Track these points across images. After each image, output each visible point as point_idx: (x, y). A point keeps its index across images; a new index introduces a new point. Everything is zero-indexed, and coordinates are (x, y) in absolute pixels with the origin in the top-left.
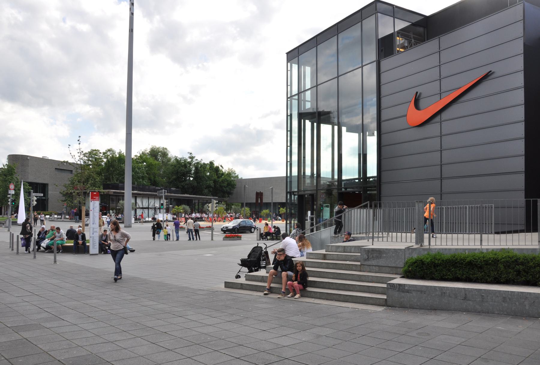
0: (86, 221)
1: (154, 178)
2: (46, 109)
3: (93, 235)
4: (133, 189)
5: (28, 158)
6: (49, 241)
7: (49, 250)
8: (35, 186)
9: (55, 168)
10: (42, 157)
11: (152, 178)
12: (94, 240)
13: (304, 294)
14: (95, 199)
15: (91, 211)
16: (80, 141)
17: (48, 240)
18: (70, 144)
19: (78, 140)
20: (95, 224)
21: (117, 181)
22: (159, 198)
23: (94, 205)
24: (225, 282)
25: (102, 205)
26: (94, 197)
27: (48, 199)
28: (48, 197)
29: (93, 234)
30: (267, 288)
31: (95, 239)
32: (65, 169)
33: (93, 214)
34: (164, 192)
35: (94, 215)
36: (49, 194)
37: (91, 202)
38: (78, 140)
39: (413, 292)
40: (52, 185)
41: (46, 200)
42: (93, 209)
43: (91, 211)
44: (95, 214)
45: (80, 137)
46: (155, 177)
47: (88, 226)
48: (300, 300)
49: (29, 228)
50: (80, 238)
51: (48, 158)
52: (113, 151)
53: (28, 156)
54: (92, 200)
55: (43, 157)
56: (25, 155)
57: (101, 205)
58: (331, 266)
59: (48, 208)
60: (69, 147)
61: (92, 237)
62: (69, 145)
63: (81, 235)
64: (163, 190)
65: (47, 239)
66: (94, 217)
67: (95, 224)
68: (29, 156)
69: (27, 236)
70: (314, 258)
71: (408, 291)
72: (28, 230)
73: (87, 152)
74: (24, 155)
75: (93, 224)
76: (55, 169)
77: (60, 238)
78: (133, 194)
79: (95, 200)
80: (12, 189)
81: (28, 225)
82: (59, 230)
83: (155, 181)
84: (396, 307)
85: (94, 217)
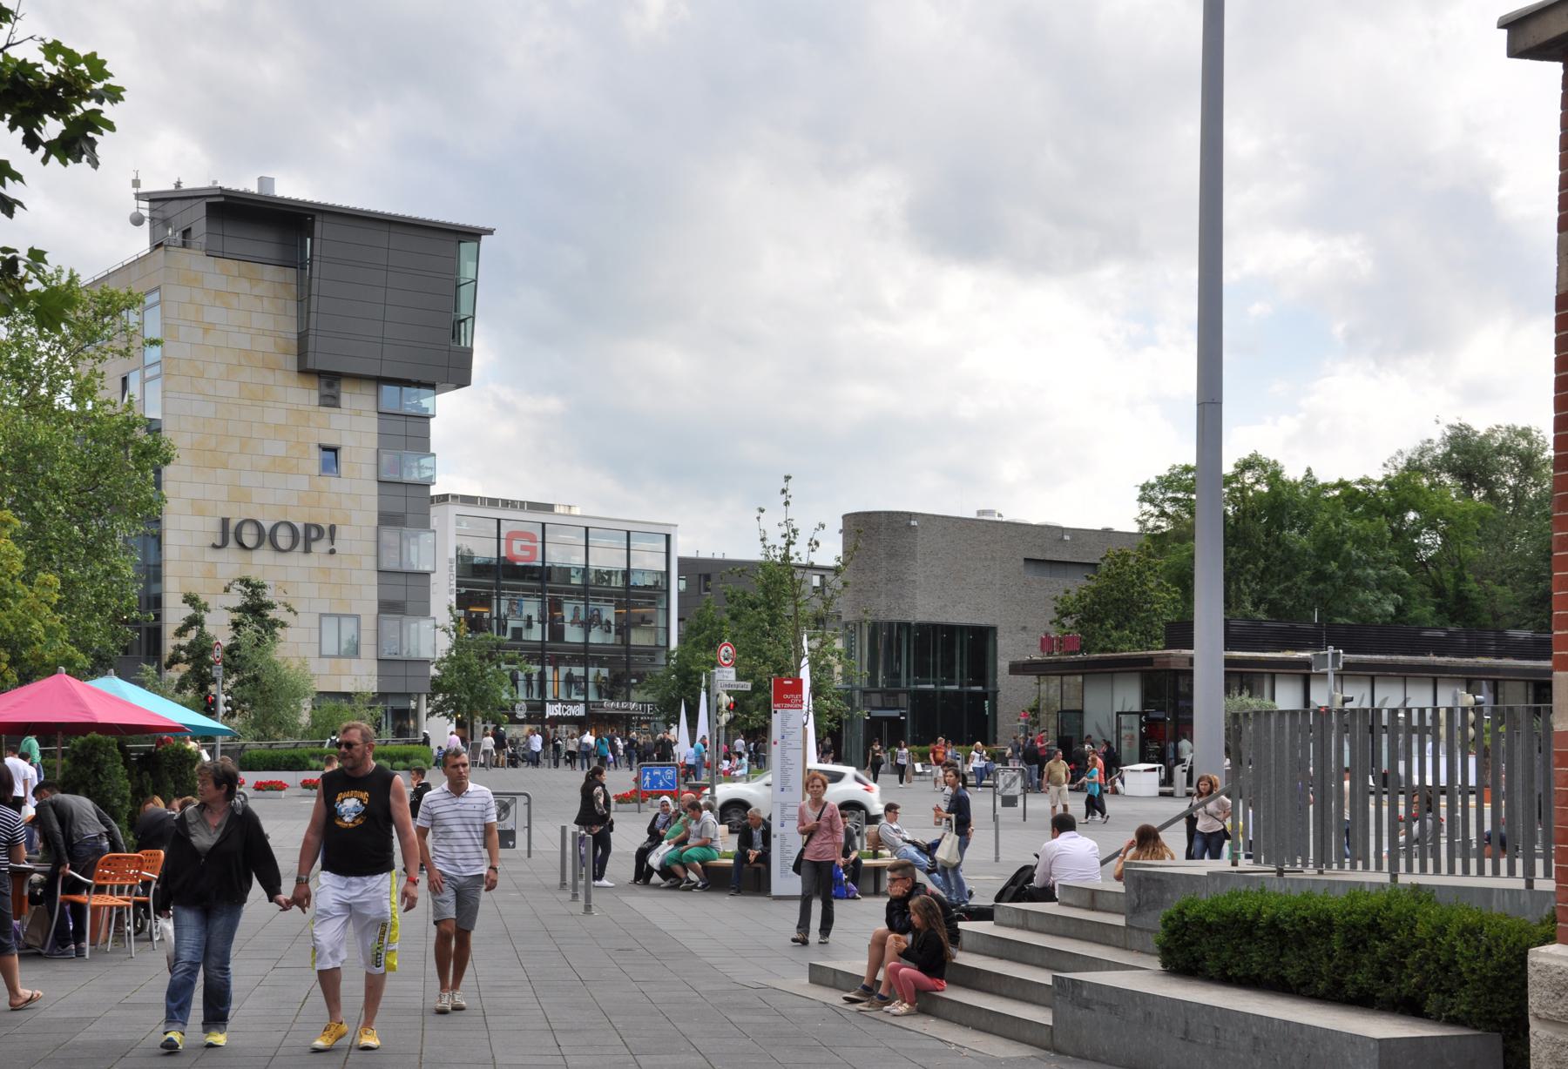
0: (1007, 786)
1: (1457, 585)
2: (1110, 273)
3: (783, 830)
4: (1231, 641)
5: (914, 523)
6: (672, 846)
7: (672, 880)
8: (969, 639)
9: (1025, 559)
10: (973, 516)
11: (1446, 585)
12: (788, 848)
13: (925, 1004)
14: (788, 701)
15: (775, 743)
16: (789, 493)
17: (669, 844)
18: (763, 507)
19: (784, 491)
20: (791, 790)
21: (1256, 605)
22: (1369, 678)
23: (784, 724)
24: (811, 964)
25: (1151, 716)
26: (786, 696)
27: (995, 693)
28: (995, 684)
29: (782, 825)
30: (864, 983)
31: (787, 843)
32: (1067, 558)
33: (783, 754)
34: (1333, 654)
35: (784, 759)
36: (999, 673)
37: (775, 712)
38: (784, 491)
39: (1096, 1007)
40: (1010, 632)
41: (990, 695)
42: (783, 737)
43: (775, 743)
44: (789, 754)
45: (788, 478)
46: (1461, 578)
47: (1013, 806)
48: (905, 1022)
49: (601, 800)
50: (756, 841)
51: (1000, 515)
52: (1264, 466)
53: (911, 515)
54: (778, 705)
55: (979, 513)
56: (902, 513)
57: (1143, 719)
58: (1033, 923)
59: (995, 732)
60: (758, 518)
61: (778, 836)
62: (762, 511)
63: (761, 828)
64: (1331, 650)
65: (665, 842)
66: (787, 766)
67: (791, 790)
68: (916, 514)
69: (597, 829)
70: (1074, 903)
71: (1086, 1005)
72: (599, 804)
73: (1153, 481)
74: (897, 513)
75: (783, 790)
76: (1022, 563)
77: (700, 837)
78: (1229, 662)
79: (788, 705)
80: (726, 662)
81: (598, 789)
82: (697, 812)
83: (1462, 598)
84: (1067, 1054)
85: (787, 766)
